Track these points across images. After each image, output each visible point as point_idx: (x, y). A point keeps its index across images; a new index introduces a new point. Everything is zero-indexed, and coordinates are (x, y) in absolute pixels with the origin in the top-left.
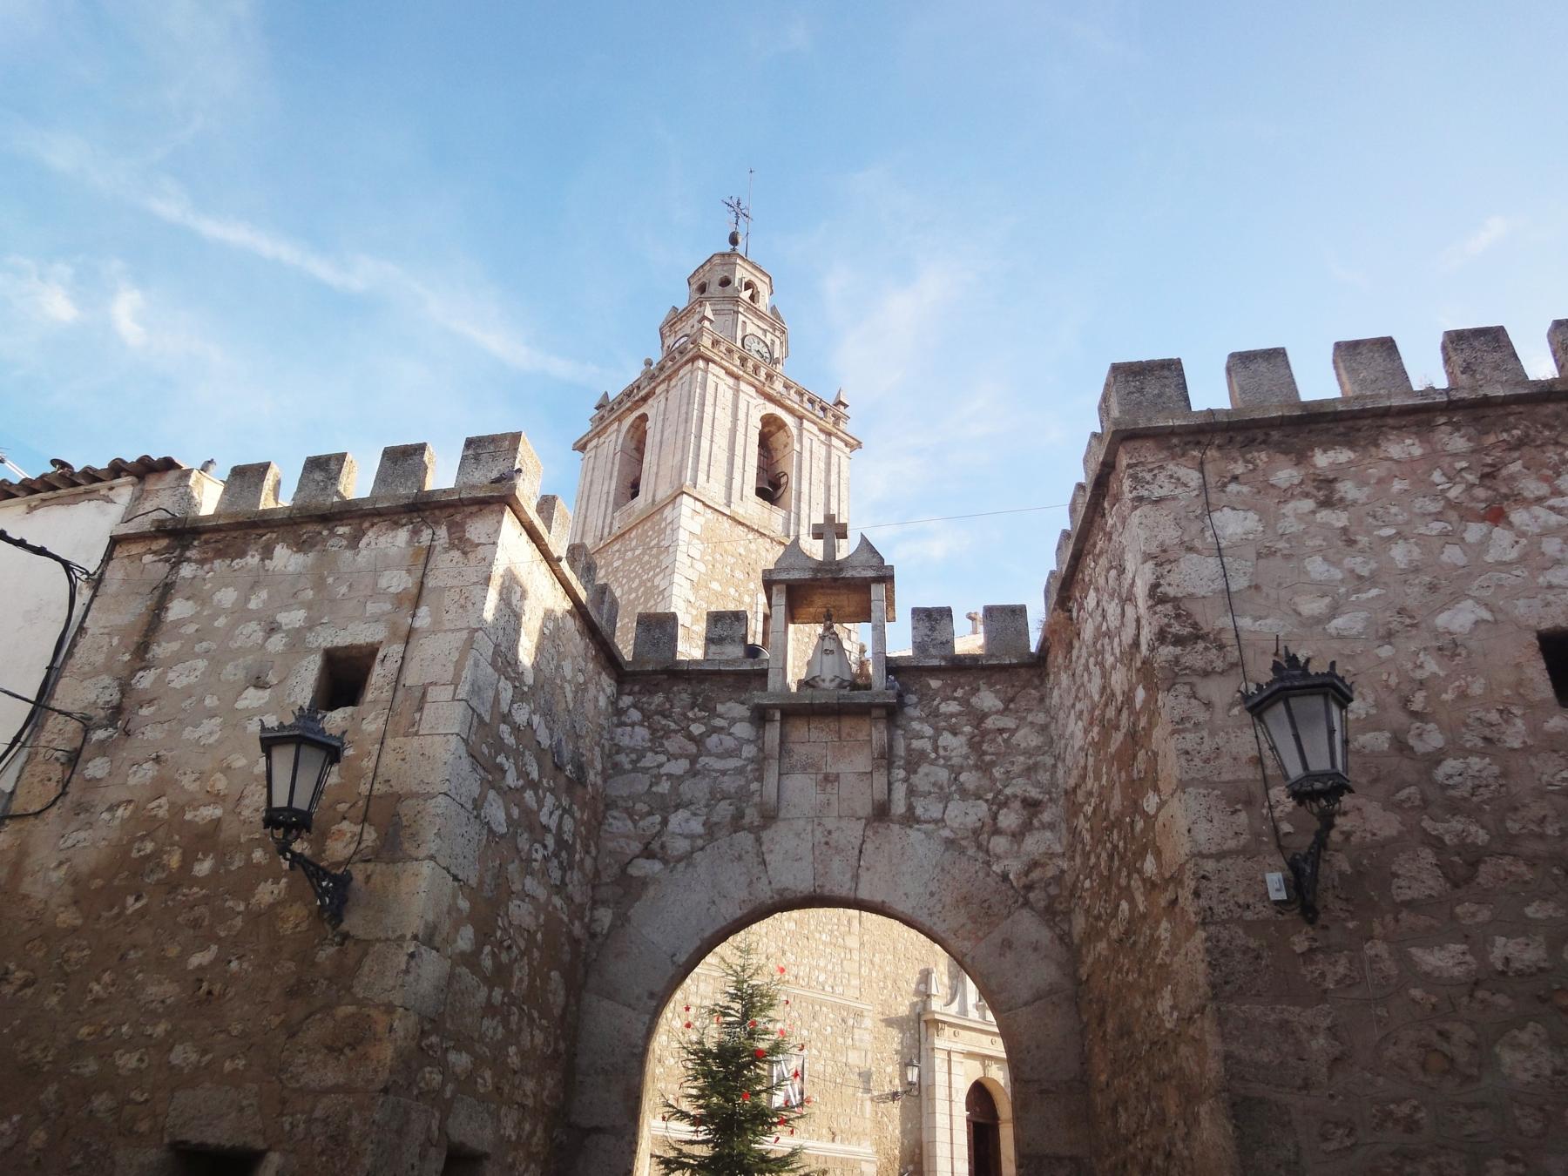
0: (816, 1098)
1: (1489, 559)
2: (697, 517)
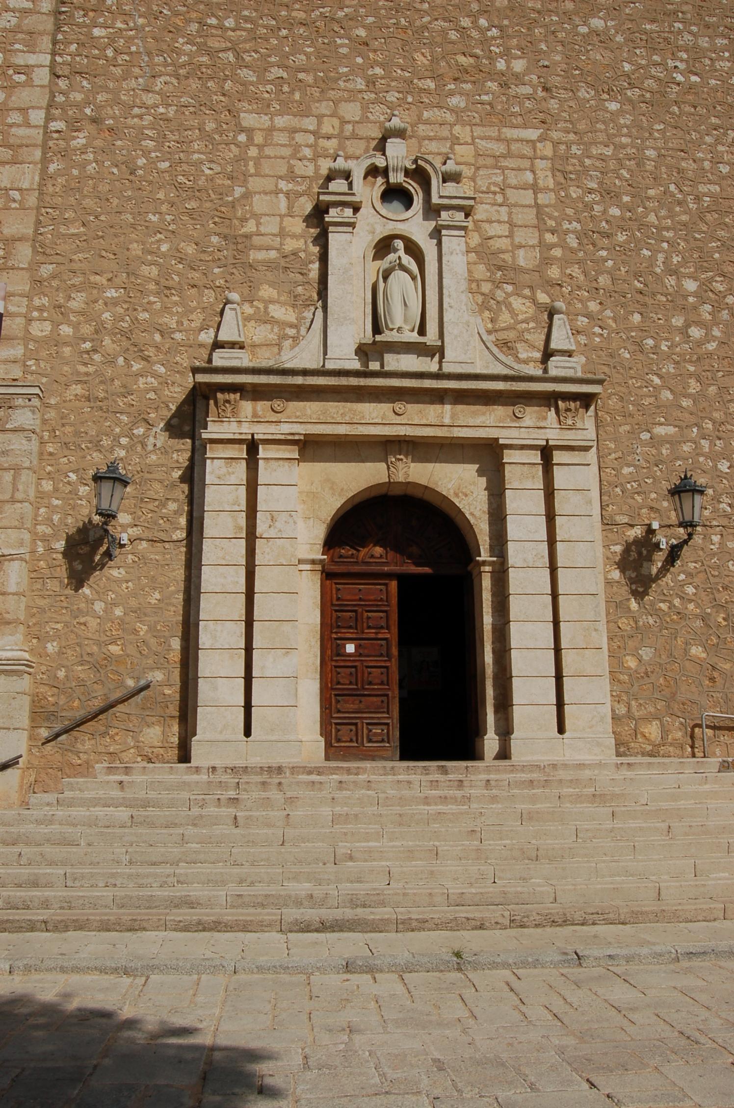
0: (297, 225)
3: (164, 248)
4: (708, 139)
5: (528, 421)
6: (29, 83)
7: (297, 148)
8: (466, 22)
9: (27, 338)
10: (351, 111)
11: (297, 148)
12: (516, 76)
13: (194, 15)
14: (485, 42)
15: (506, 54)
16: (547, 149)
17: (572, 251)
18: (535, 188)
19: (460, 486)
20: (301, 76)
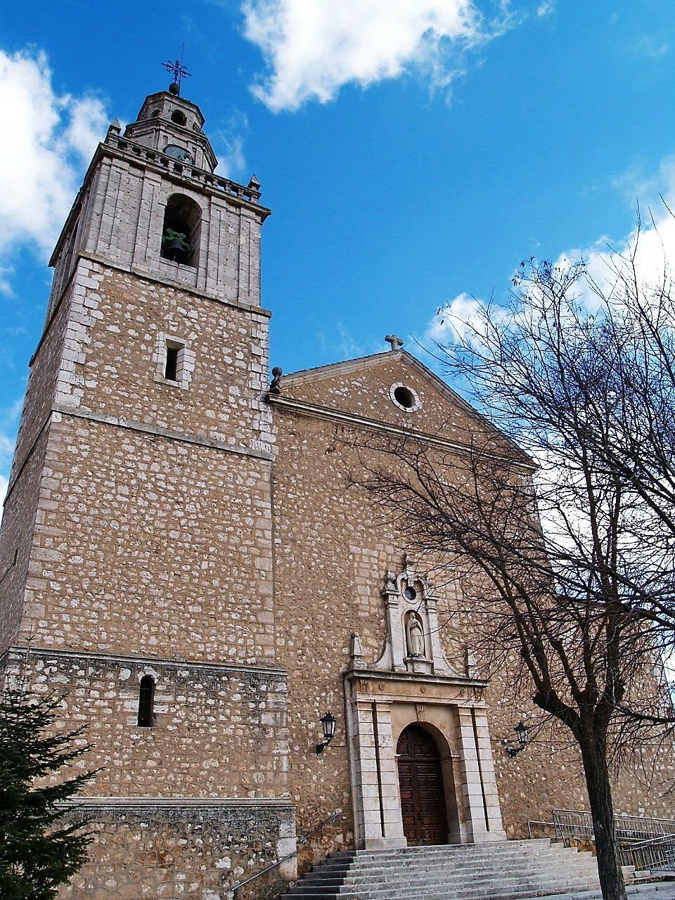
6: (263, 516)
11: (372, 565)
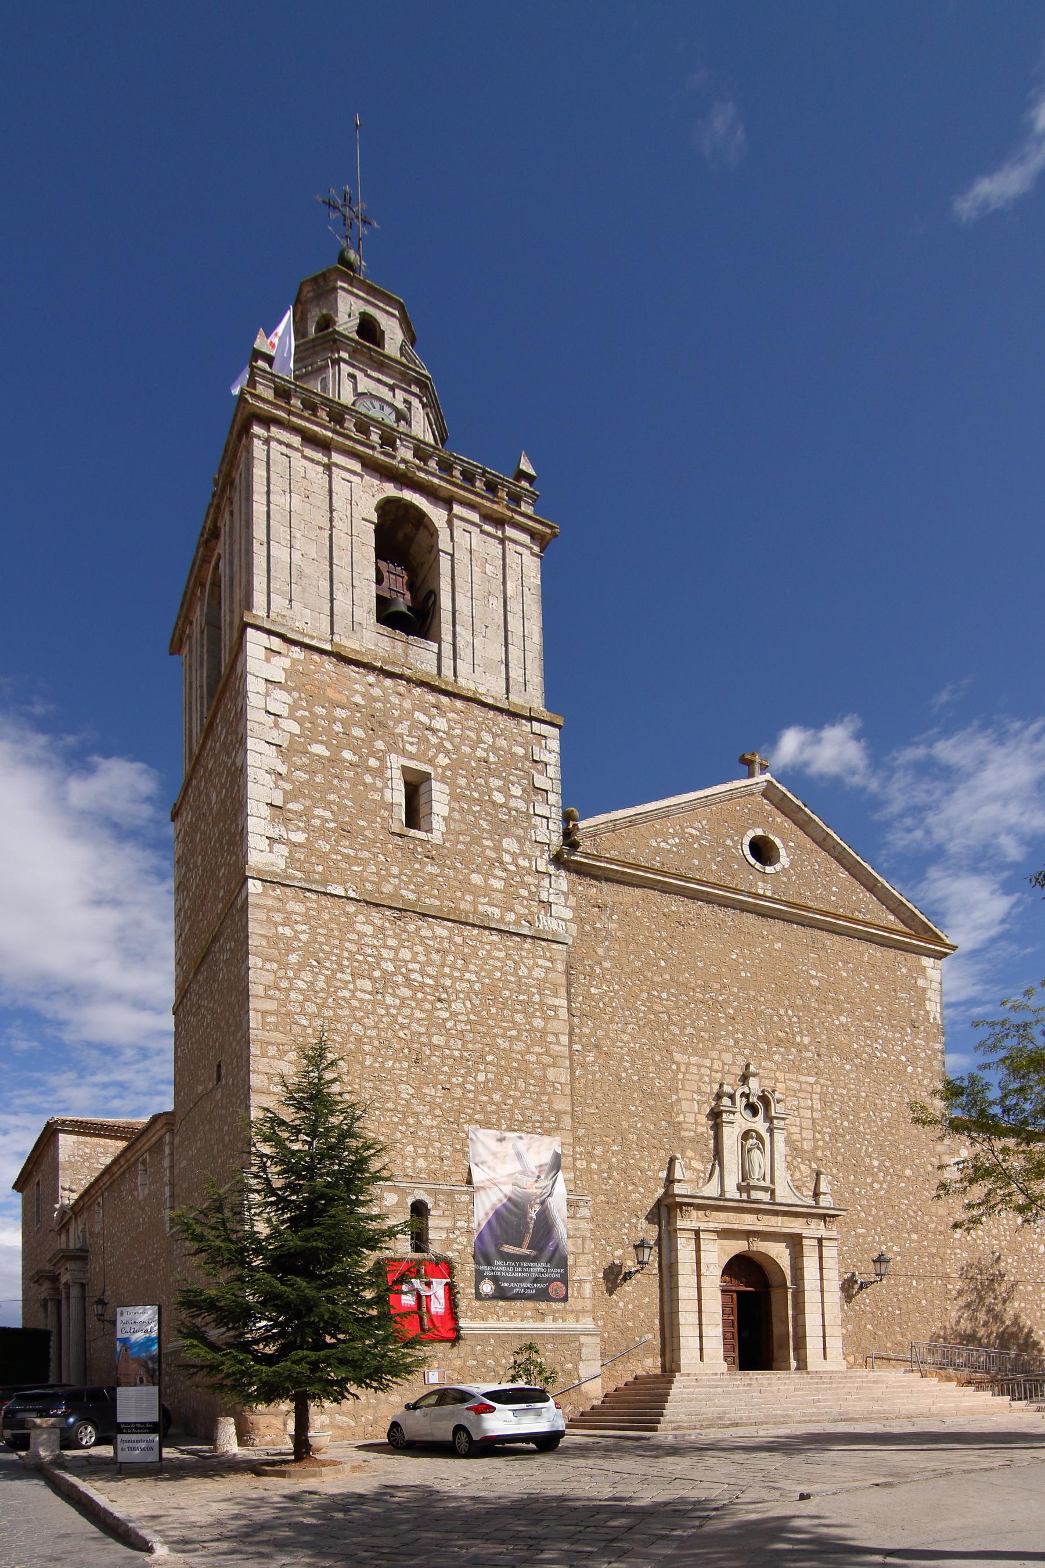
0: (703, 1119)
1: (122, 1144)
2: (276, 659)
3: (639, 1125)
4: (888, 1089)
5: (812, 1226)
7: (702, 1076)
8: (782, 1012)
9: (575, 1169)
10: (727, 1057)
11: (702, 1076)
12: (805, 1046)
13: (645, 988)
14: (791, 1025)
15: (801, 1032)
16: (817, 1089)
17: (827, 1143)
18: (812, 1109)
19: (779, 1253)
20: (702, 1034)
